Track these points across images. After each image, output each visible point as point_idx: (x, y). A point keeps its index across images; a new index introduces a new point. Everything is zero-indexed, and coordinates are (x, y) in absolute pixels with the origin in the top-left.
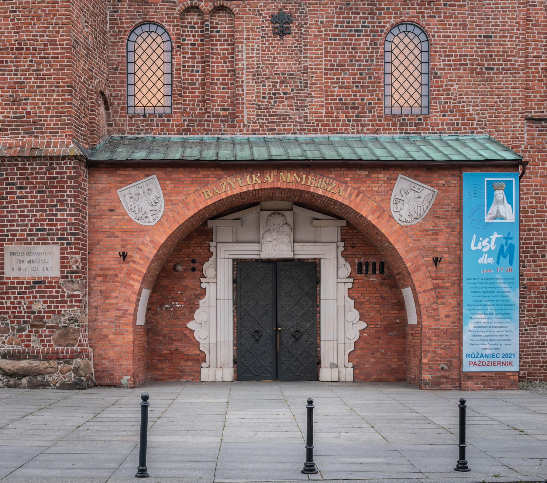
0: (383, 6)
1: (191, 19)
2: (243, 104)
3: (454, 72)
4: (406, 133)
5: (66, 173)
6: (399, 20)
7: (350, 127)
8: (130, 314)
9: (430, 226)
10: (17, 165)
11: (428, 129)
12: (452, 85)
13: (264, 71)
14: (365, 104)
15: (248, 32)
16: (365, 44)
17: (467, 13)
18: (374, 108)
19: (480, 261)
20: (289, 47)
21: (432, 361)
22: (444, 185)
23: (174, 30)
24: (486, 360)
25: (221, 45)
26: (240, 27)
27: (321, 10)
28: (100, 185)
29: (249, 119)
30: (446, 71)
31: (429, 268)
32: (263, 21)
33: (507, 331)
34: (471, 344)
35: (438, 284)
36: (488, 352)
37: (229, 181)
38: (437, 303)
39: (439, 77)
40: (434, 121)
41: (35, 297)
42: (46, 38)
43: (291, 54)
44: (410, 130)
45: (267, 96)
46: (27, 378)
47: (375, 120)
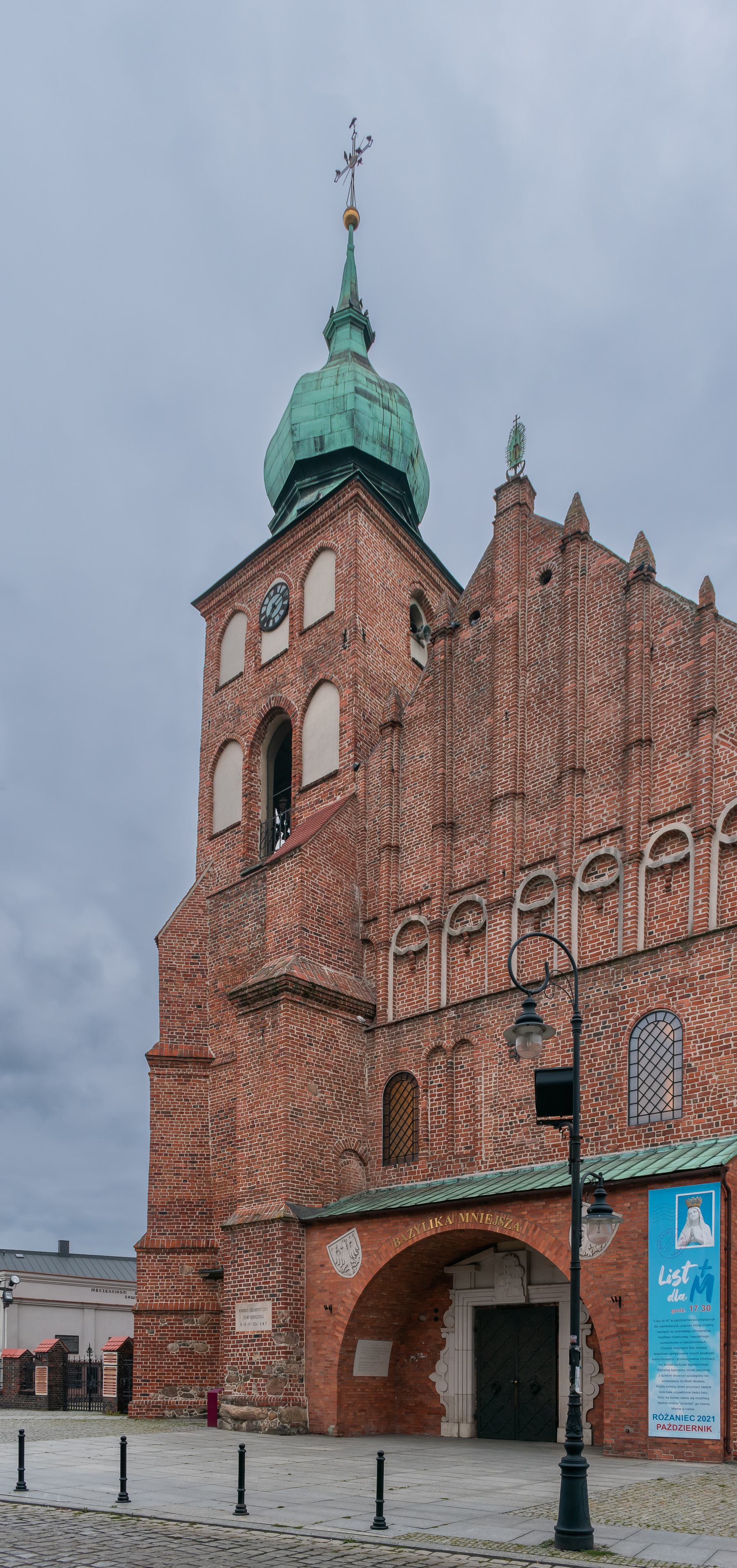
0: (626, 998)
1: (438, 1059)
2: (481, 1139)
3: (713, 1059)
4: (652, 1145)
5: (275, 1234)
6: (644, 1010)
7: (589, 1148)
8: (335, 1365)
9: (612, 1259)
10: (244, 1231)
11: (679, 1136)
12: (710, 1077)
13: (501, 1100)
14: (606, 1118)
15: (486, 1061)
16: (606, 1047)
17: (730, 980)
18: (615, 1121)
19: (670, 1298)
20: (525, 1069)
21: (616, 1421)
22: (629, 1208)
23: (420, 1075)
24: (677, 1423)
25: (465, 1080)
26: (479, 1057)
27: (558, 1020)
28: (315, 1243)
29: (487, 1154)
30: (703, 1060)
31: (612, 1310)
32: (500, 1047)
33: (704, 1387)
34: (659, 1403)
35: (622, 1328)
36: (680, 1413)
37: (415, 1227)
38: (621, 1351)
39: (695, 1069)
40: (687, 1126)
41: (255, 1349)
42: (270, 1113)
43: (527, 1076)
44: (658, 1140)
45: (504, 1127)
46: (246, 1422)
47: (616, 1136)
